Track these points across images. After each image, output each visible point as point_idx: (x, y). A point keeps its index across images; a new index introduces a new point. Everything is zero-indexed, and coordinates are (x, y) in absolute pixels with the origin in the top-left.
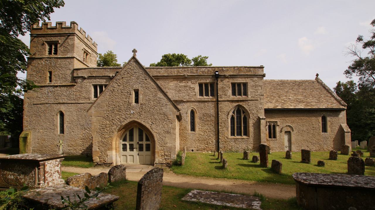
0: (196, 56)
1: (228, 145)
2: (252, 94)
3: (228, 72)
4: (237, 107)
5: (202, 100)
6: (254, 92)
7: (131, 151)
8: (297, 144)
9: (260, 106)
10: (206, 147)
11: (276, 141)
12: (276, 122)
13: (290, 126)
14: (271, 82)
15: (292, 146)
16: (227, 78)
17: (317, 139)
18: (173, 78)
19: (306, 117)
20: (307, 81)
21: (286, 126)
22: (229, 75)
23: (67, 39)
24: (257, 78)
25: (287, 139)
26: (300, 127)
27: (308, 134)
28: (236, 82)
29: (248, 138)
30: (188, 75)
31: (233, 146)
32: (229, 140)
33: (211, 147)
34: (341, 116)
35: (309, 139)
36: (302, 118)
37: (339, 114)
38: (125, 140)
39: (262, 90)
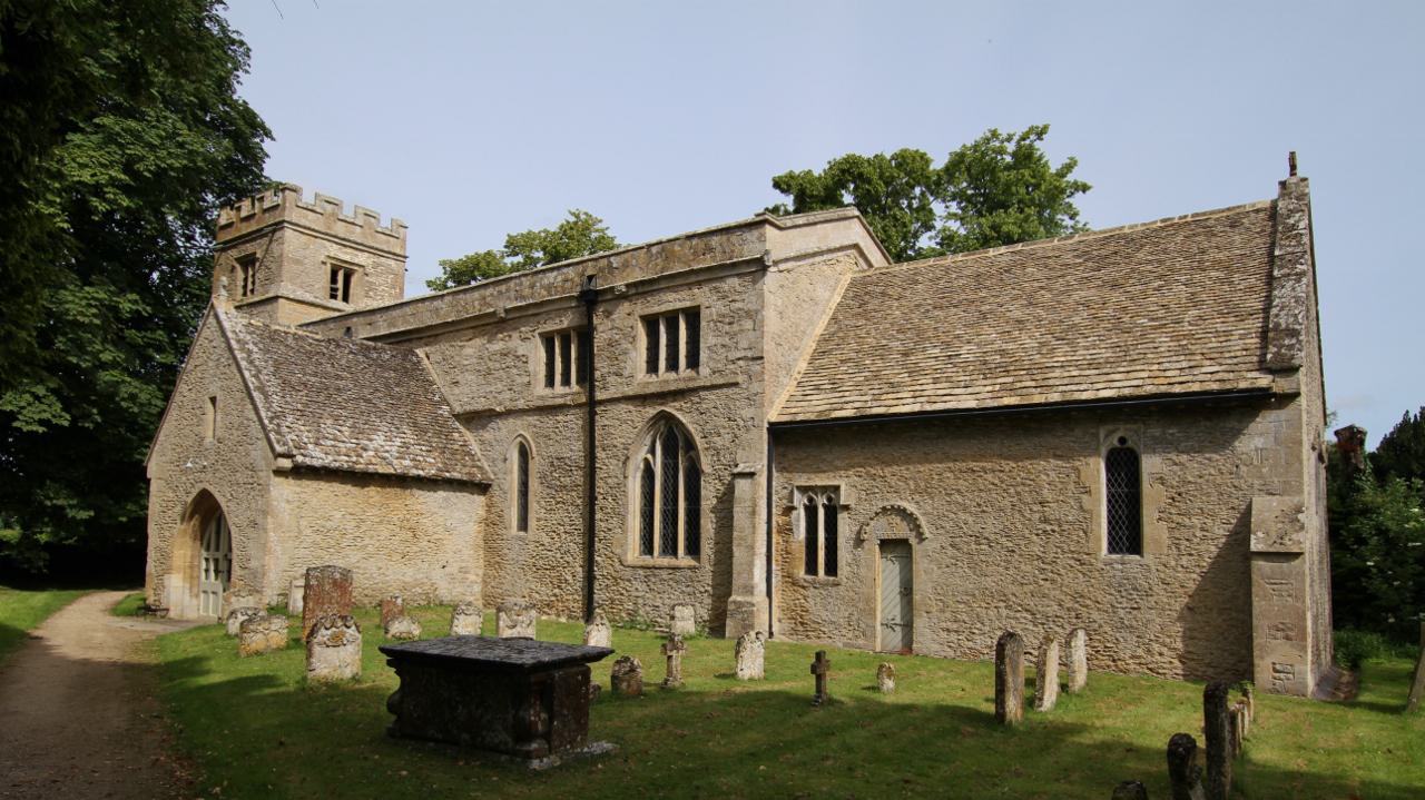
0: (896, 150)
1: (622, 594)
2: (715, 356)
3: (628, 270)
4: (663, 422)
5: (547, 404)
6: (724, 346)
8: (948, 615)
9: (747, 413)
10: (555, 595)
11: (833, 590)
12: (837, 489)
13: (902, 512)
14: (1121, 245)
15: (920, 623)
16: (624, 297)
17: (1067, 594)
18: (472, 328)
19: (1001, 456)
20: (1170, 227)
21: (884, 509)
22: (627, 286)
23: (271, 242)
24: (738, 275)
26: (963, 516)
27: (1008, 562)
28: (656, 309)
29: (695, 568)
30: (506, 311)
31: (640, 601)
32: (628, 573)
33: (570, 597)
34: (1258, 442)
35: (1014, 589)
36: (972, 465)
37: (1237, 433)
38: (208, 549)
39: (758, 332)
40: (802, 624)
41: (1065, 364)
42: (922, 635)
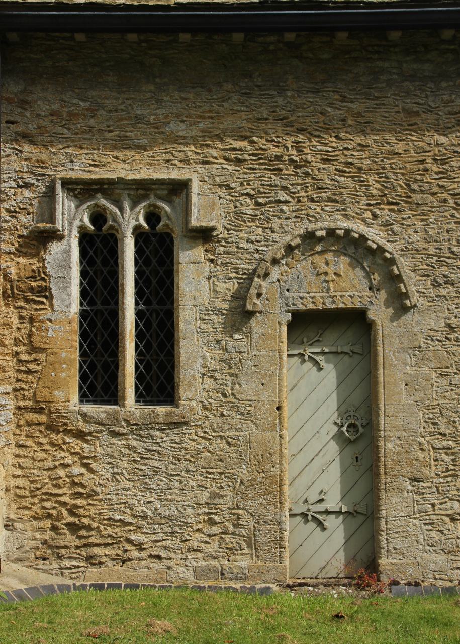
7: (373, 321)
11: (166, 440)
12: (179, 188)
21: (310, 238)
25: (333, 404)
40: (74, 528)
41: (446, 484)
42: (406, 535)
